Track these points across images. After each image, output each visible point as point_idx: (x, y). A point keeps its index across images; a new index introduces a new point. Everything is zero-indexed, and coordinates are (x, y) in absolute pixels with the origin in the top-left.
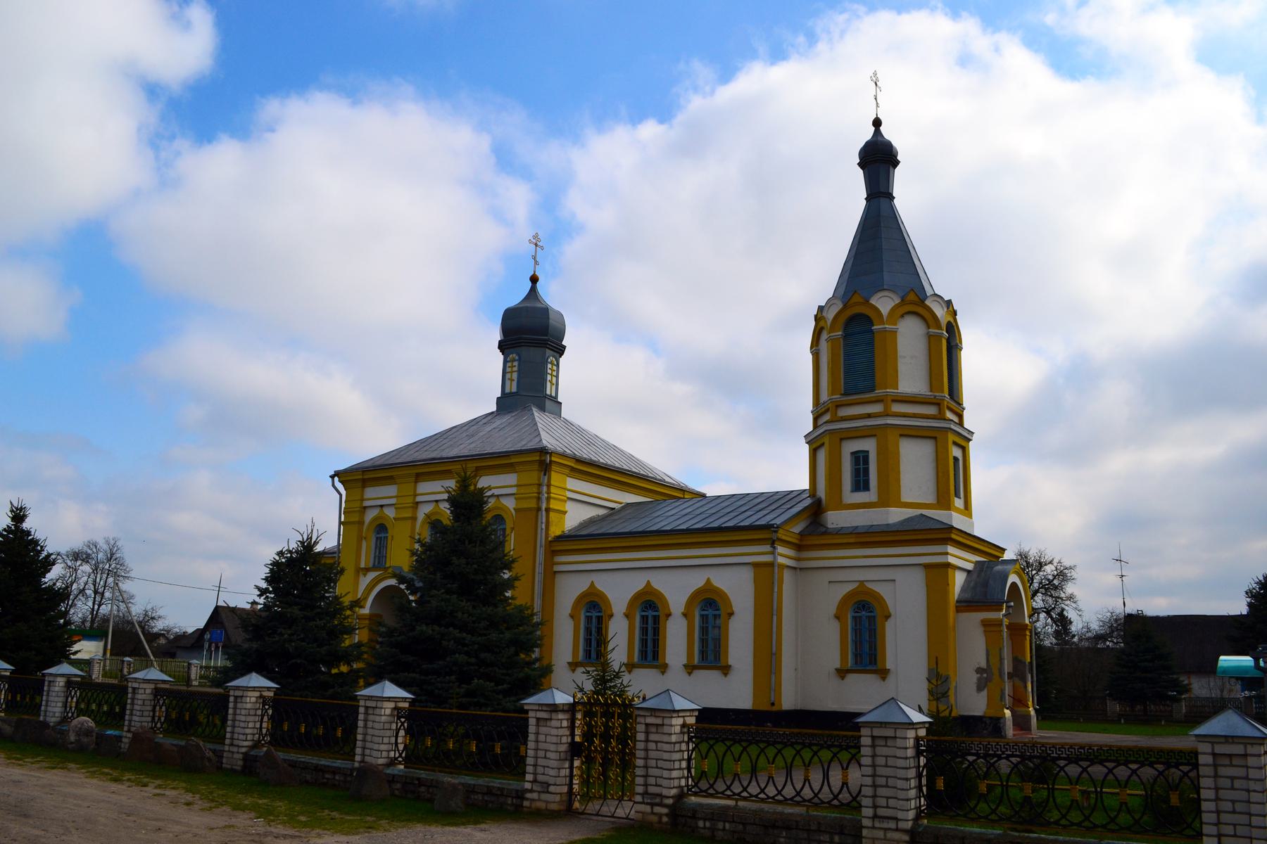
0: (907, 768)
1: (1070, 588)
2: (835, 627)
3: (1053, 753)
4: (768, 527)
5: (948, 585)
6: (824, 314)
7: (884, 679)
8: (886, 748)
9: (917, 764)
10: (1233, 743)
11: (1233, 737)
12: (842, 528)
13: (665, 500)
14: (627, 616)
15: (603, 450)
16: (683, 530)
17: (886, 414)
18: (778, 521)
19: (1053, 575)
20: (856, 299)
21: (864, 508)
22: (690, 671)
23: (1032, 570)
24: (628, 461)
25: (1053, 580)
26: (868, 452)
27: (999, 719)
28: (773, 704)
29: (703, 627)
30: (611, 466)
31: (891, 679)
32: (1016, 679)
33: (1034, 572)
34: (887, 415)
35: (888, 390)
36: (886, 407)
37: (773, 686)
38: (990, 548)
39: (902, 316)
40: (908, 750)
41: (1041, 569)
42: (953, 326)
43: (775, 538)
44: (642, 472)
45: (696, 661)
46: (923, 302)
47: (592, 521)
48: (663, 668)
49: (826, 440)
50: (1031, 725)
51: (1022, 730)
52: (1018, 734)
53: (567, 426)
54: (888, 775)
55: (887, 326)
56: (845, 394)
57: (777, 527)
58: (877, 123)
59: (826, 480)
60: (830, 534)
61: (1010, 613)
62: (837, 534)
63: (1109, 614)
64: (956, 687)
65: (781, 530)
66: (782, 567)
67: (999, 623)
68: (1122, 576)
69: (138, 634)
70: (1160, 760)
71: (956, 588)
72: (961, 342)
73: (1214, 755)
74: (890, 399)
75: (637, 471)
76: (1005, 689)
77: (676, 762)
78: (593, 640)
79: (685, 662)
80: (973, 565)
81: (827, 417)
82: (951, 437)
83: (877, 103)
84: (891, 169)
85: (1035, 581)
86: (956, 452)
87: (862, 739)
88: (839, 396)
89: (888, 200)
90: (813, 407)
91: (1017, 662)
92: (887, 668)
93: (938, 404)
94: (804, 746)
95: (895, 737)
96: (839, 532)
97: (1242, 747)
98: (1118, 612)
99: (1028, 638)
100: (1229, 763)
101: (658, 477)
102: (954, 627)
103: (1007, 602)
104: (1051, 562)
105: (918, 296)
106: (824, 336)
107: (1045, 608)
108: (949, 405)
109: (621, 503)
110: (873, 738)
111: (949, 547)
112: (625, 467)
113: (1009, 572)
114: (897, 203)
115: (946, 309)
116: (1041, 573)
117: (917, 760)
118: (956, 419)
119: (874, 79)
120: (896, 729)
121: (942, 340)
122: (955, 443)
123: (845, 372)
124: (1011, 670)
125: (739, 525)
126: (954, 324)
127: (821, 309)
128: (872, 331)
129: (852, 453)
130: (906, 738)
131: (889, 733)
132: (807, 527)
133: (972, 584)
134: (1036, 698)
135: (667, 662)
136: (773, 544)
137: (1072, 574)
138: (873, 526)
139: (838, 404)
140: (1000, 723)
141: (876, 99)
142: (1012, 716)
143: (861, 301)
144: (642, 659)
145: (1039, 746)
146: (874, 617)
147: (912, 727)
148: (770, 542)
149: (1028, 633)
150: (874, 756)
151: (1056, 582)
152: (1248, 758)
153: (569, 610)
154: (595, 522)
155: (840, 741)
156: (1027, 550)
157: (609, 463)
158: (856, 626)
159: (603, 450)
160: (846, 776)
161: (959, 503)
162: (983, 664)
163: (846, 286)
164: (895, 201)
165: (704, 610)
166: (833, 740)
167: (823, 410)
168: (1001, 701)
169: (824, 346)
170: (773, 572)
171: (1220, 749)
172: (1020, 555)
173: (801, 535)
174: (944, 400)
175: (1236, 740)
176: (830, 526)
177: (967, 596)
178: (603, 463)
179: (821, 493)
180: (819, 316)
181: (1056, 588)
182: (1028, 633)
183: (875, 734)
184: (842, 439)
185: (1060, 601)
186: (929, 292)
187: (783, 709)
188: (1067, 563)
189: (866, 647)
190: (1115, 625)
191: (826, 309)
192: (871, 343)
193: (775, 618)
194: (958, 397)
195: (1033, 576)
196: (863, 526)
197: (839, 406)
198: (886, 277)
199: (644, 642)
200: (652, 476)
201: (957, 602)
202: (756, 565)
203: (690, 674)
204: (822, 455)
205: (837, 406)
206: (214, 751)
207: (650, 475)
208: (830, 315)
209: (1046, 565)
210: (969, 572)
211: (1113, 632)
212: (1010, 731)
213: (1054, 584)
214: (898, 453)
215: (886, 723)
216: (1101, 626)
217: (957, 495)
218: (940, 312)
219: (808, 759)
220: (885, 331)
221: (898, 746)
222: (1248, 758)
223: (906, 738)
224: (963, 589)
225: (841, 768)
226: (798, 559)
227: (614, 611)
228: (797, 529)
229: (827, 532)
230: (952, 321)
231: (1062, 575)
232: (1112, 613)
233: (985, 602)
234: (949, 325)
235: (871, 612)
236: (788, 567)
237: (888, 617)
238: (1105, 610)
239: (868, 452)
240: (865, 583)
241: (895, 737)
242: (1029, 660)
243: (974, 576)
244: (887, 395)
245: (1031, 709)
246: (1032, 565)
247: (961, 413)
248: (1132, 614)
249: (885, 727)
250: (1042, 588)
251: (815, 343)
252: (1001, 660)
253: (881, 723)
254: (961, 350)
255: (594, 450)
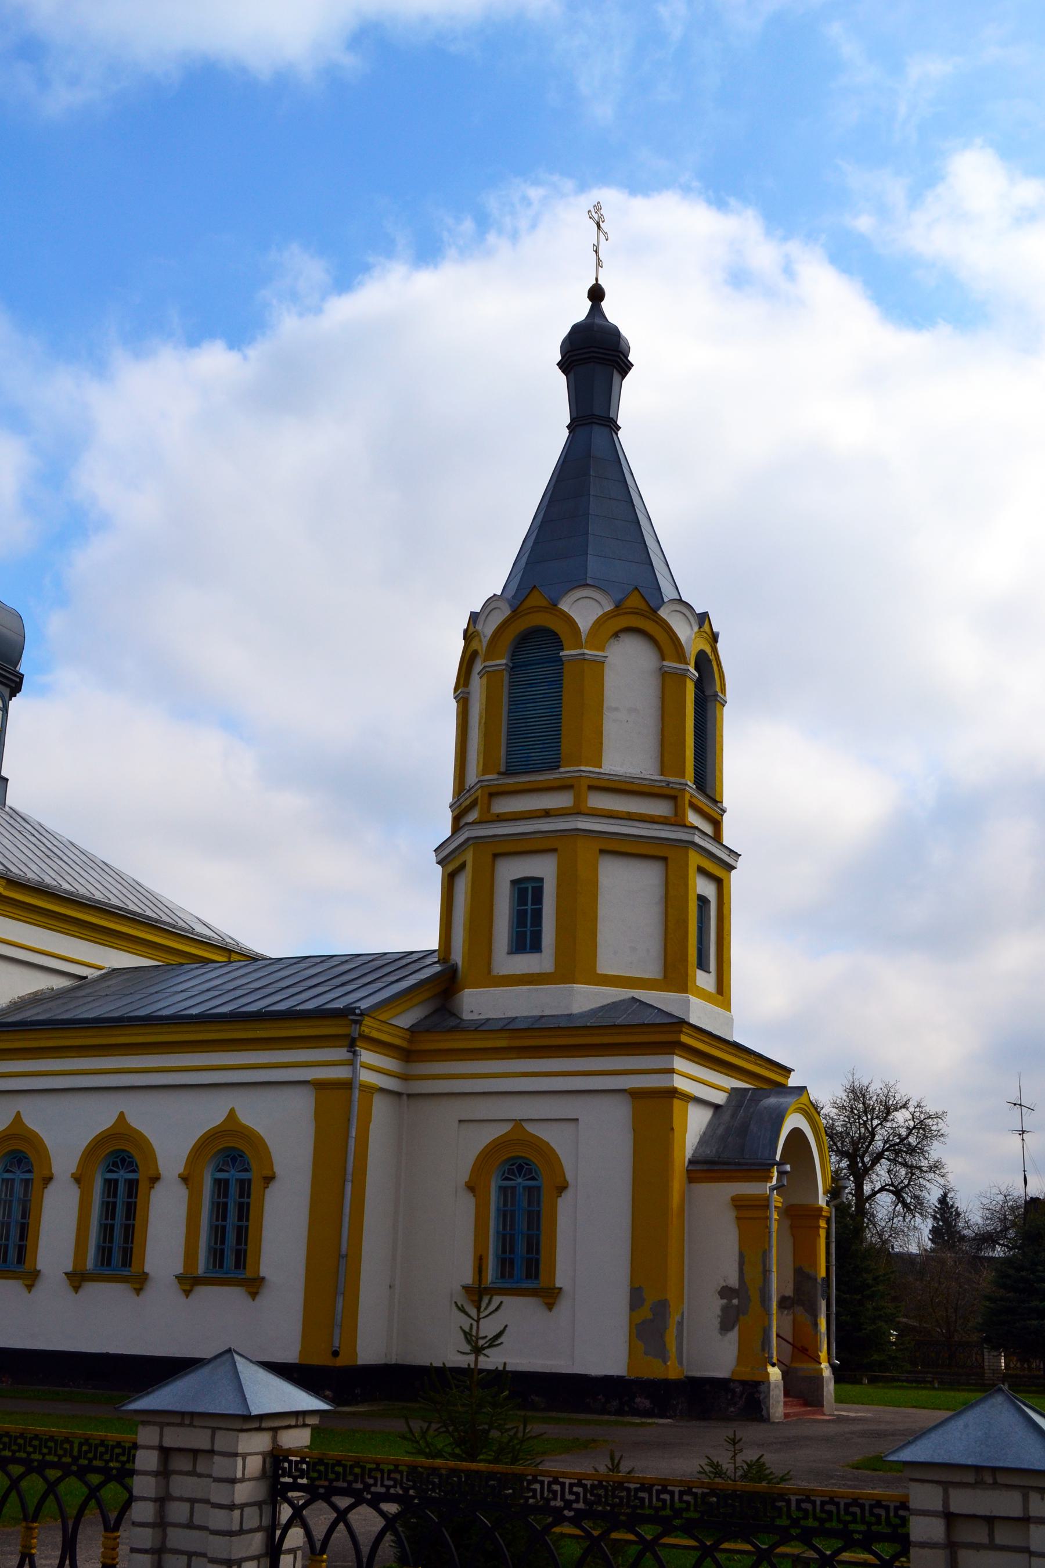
0: (230, 1534)
1: (936, 1151)
2: (467, 1204)
3: (555, 1499)
4: (346, 1014)
5: (672, 1129)
6: (479, 627)
7: (550, 1306)
8: (195, 1479)
9: (266, 1521)
10: (995, 1485)
11: (994, 1470)
12: (488, 1020)
13: (182, 964)
14: (77, 1179)
15: (77, 868)
16: (191, 1016)
17: (577, 811)
18: (364, 1005)
19: (907, 1128)
20: (535, 600)
21: (530, 983)
22: (188, 1288)
23: (872, 1119)
24: (124, 891)
25: (907, 1137)
26: (541, 880)
27: (757, 1384)
28: (336, 1354)
29: (218, 1203)
30: (89, 899)
31: (563, 1306)
32: (799, 1309)
33: (876, 1122)
34: (579, 813)
35: (583, 768)
36: (578, 799)
37: (339, 1317)
38: (760, 1066)
39: (616, 635)
40: (238, 1487)
41: (886, 1117)
42: (710, 661)
43: (357, 1036)
44: (149, 913)
45: (201, 1270)
46: (656, 612)
47: (36, 999)
48: (140, 1282)
49: (469, 857)
50: (822, 1395)
51: (806, 1404)
52: (795, 1414)
53: (12, 822)
54: (192, 1550)
55: (586, 651)
56: (507, 773)
57: (361, 1015)
58: (596, 294)
59: (464, 930)
60: (464, 1030)
61: (784, 1185)
62: (476, 1030)
63: (1001, 1197)
64: (680, 1324)
65: (367, 1018)
66: (370, 1090)
67: (764, 1204)
68: (1023, 1132)
69: (777, 1320)
70: (828, 1525)
71: (688, 1136)
72: (723, 690)
73: (950, 1518)
74: (584, 783)
75: (140, 911)
76: (770, 1327)
77: (249, 1459)
78: (12, 1225)
79: (179, 1269)
80: (726, 1095)
81: (473, 816)
82: (695, 859)
83: (599, 260)
84: (616, 376)
85: (877, 1138)
86: (705, 888)
87: (140, 1454)
88: (495, 776)
89: (606, 430)
90: (454, 798)
91: (802, 1277)
92: (558, 1285)
93: (673, 797)
94: (31, 1468)
95: (212, 1452)
96: (481, 1027)
97: (1017, 1497)
98: (1016, 1194)
99: (823, 1233)
100: (985, 1540)
101: (181, 924)
102: (682, 1210)
103: (779, 1164)
104: (905, 1106)
105: (646, 602)
106: (478, 666)
107: (892, 1185)
108: (694, 800)
109: (100, 968)
110: (165, 1453)
111: (676, 1058)
112: (115, 901)
113: (786, 1109)
114: (626, 437)
115: (696, 629)
116: (888, 1124)
117: (267, 1510)
118: (708, 829)
119: (596, 216)
120: (214, 1430)
121: (686, 681)
122: (702, 871)
123: (510, 733)
124: (789, 1292)
125: (298, 1008)
126: (712, 657)
127: (474, 617)
128: (560, 660)
129: (514, 882)
130: (236, 1455)
131: (199, 1439)
132: (426, 1017)
133: (720, 1131)
134: (834, 1345)
135: (38, 1268)
136: (352, 1044)
137: (940, 1126)
138: (543, 1017)
139: (494, 790)
140: (759, 1392)
141: (596, 252)
142: (784, 1378)
143: (544, 603)
144: (102, 1264)
145: (567, 1481)
146: (539, 1188)
147: (256, 1425)
148: (347, 1043)
149: (823, 1224)
150: (162, 1501)
151: (912, 1140)
152: (1032, 1527)
153: (180, 1167)
154: (42, 1000)
155: (107, 1457)
156: (866, 1084)
157: (82, 891)
158: (505, 1205)
159: (77, 868)
160: (114, 1549)
161: (705, 981)
162: (733, 1281)
163: (521, 579)
164: (620, 433)
165: (507, 1179)
166: (107, 1457)
167: (468, 802)
168: (763, 1350)
169: (478, 685)
170: (350, 1102)
171: (962, 1502)
172: (853, 1091)
173: (412, 1032)
174: (684, 790)
175: (1001, 1479)
176: (467, 1016)
177: (710, 1152)
178: (66, 891)
179: (458, 956)
180: (470, 632)
181: (912, 1150)
182: (823, 1224)
183: (168, 1443)
184: (496, 856)
185: (917, 1172)
186: (668, 593)
187: (360, 1361)
188: (931, 1108)
189: (521, 1247)
190: (1010, 1217)
191: (482, 618)
192: (557, 682)
193: (349, 1187)
194: (714, 789)
195: (873, 1129)
196: (526, 1018)
197: (493, 795)
198: (593, 564)
199: (218, 1233)
200: (169, 920)
201: (690, 1162)
202: (320, 1086)
203: (187, 1293)
204: (463, 884)
205: (492, 795)
206: (479, 1374)
207: (165, 918)
208: (488, 629)
209: (896, 1110)
210: (717, 1107)
211: (1006, 1229)
212: (777, 1406)
213: (909, 1144)
214: (594, 883)
215: (192, 1414)
216: (987, 1219)
217: (702, 964)
218: (684, 631)
219: (36, 1501)
220: (582, 659)
221: (215, 1475)
222: (1032, 1527)
223: (236, 1455)
224: (704, 1140)
225: (102, 1527)
226: (404, 1078)
227: (54, 1170)
228: (406, 1020)
229: (460, 1027)
230: (708, 650)
231: (922, 1127)
232: (1005, 1196)
233: (739, 1164)
234: (701, 655)
235: (533, 1179)
236: (382, 1090)
237: (562, 1188)
238: (995, 1191)
239: (541, 880)
240: (524, 1124)
241: (212, 1452)
242: (823, 1273)
243: (726, 1116)
244: (581, 776)
245: (824, 1365)
246: (873, 1109)
247: (718, 817)
248: (1037, 1199)
249: (191, 1425)
250: (887, 1150)
251: (462, 682)
252: (766, 1272)
253: (183, 1414)
254: (723, 704)
255: (55, 867)
